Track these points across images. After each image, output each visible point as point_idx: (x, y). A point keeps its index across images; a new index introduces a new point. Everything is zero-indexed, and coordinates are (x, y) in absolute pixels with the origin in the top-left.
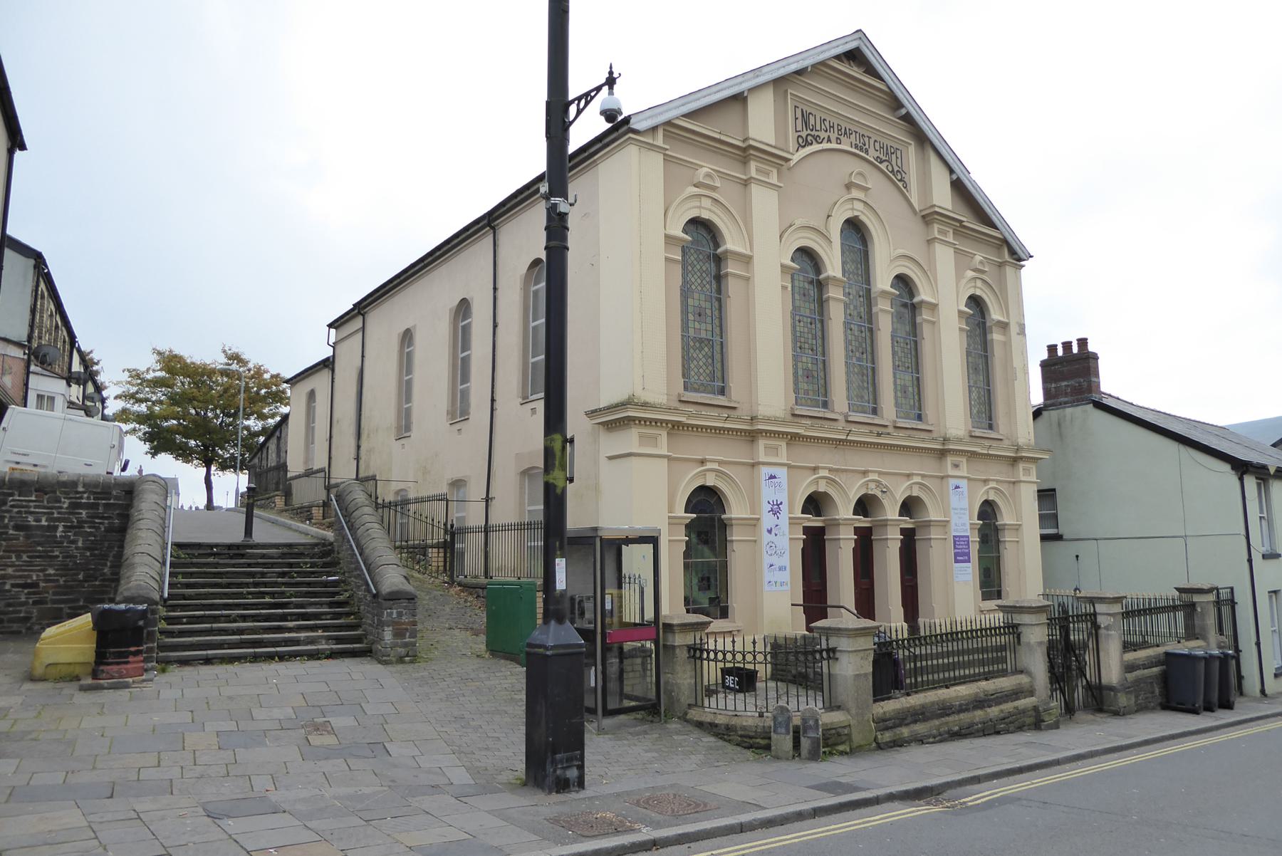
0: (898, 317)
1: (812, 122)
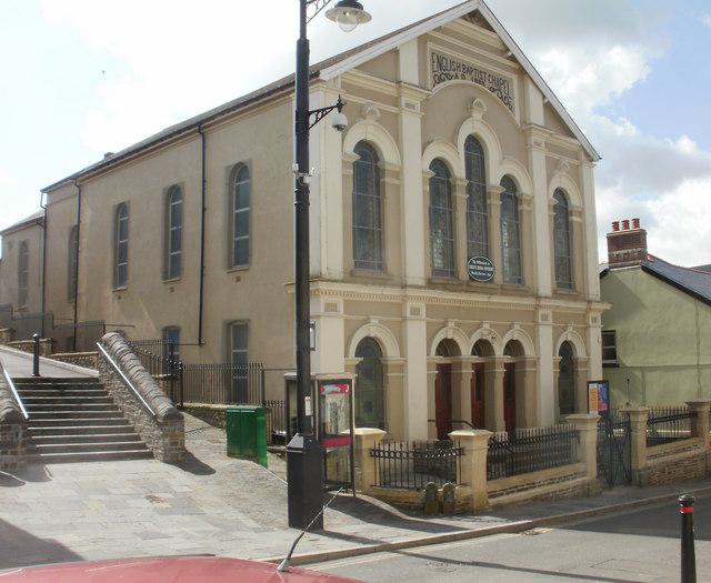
0: (504, 208)
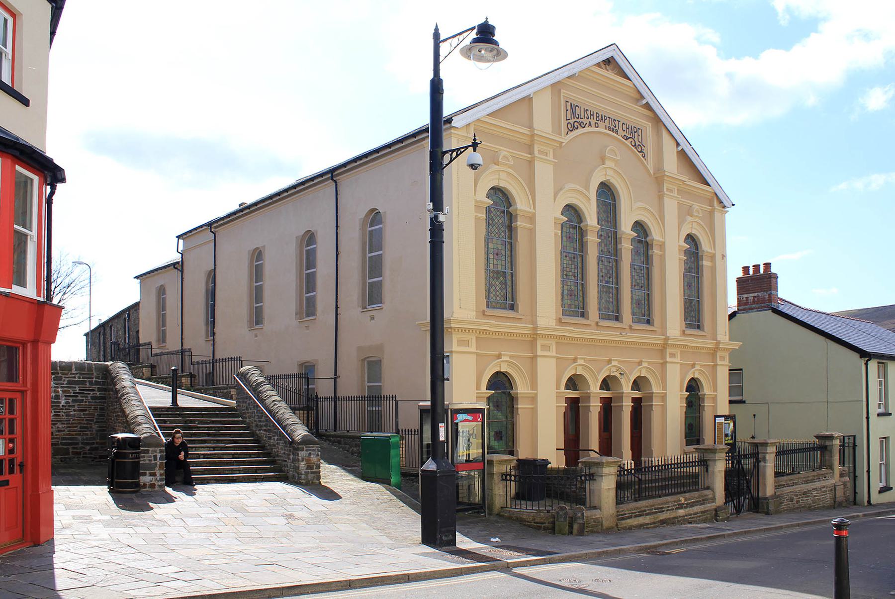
0: (636, 252)
1: (578, 112)
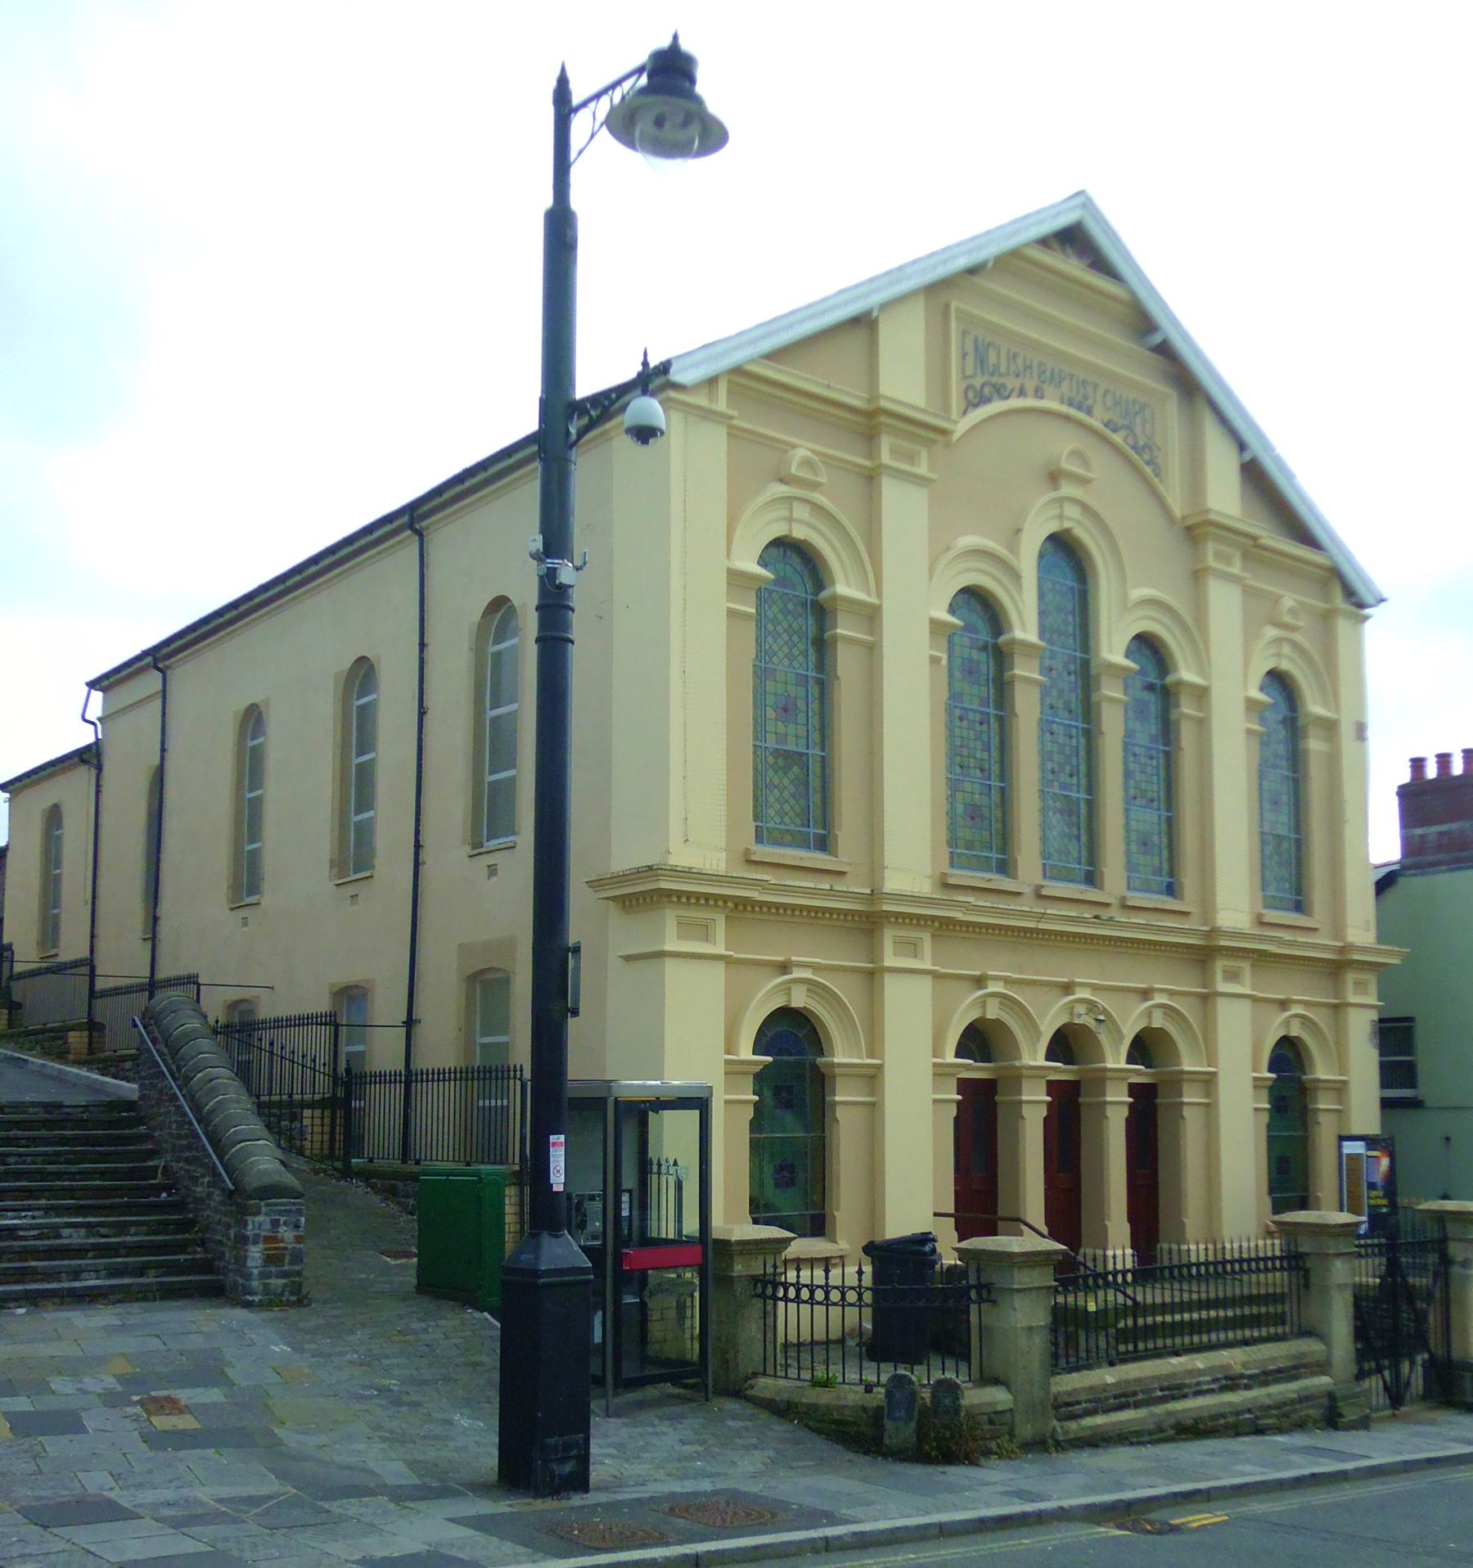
0: (1138, 711)
1: (992, 358)
